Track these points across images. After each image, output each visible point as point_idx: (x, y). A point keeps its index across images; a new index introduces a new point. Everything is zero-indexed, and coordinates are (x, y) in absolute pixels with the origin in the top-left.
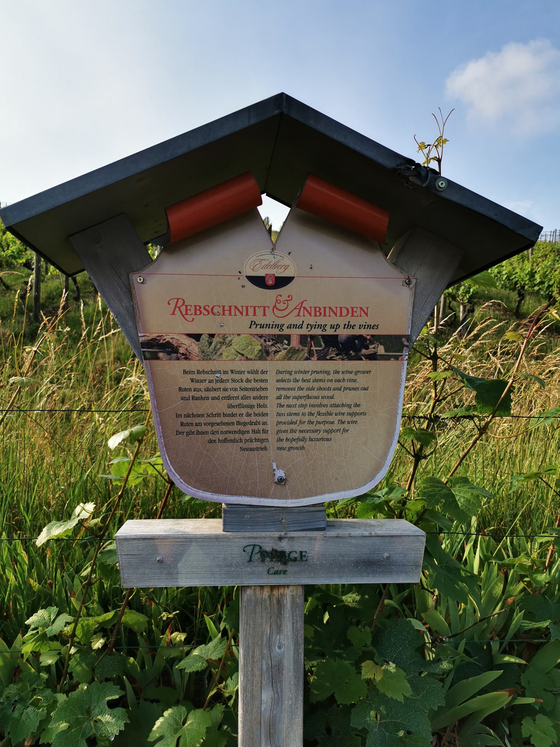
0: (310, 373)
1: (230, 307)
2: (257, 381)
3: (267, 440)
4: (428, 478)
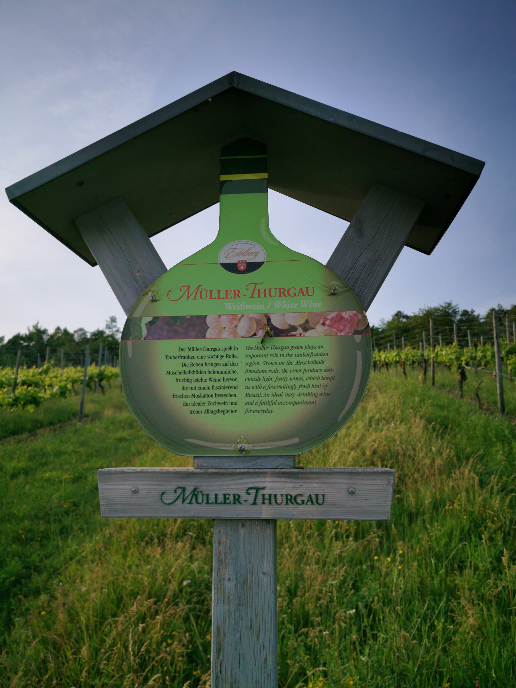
1: (265, 290)
2: (218, 396)
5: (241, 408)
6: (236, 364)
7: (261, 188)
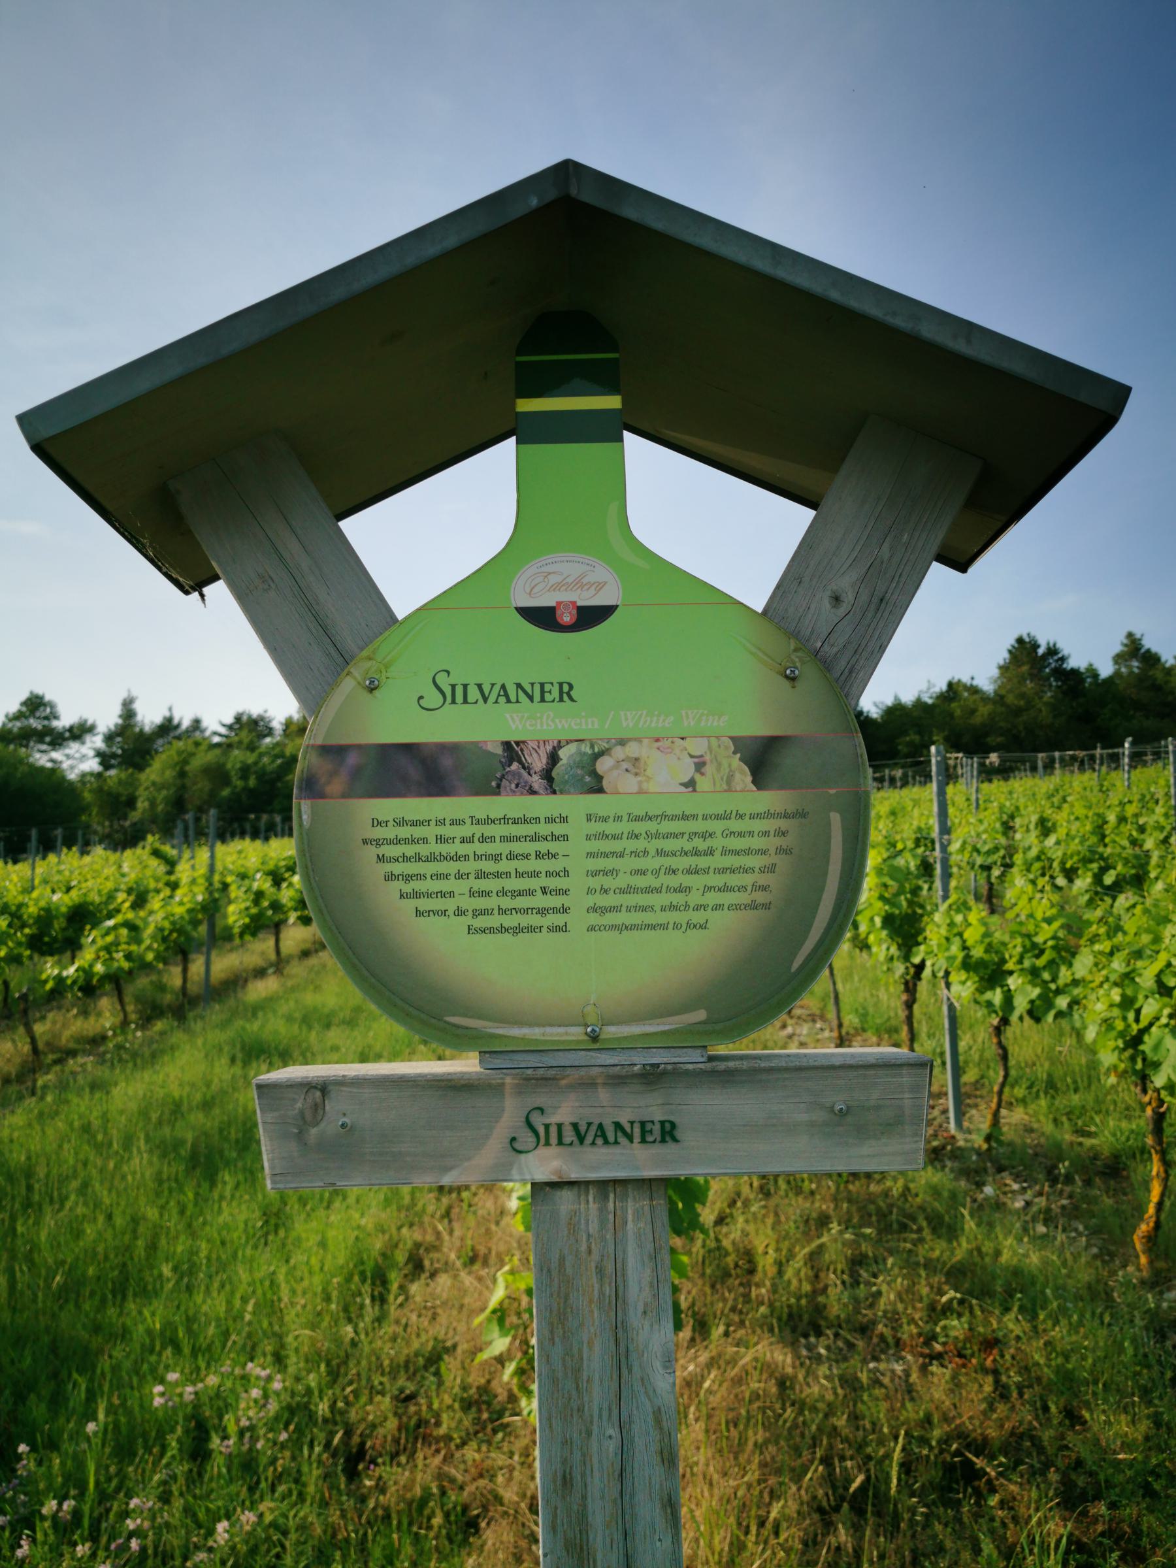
0: (686, 836)
3: (566, 873)
4: (256, 1125)
5: (578, 920)
6: (565, 838)
7: (606, 430)
